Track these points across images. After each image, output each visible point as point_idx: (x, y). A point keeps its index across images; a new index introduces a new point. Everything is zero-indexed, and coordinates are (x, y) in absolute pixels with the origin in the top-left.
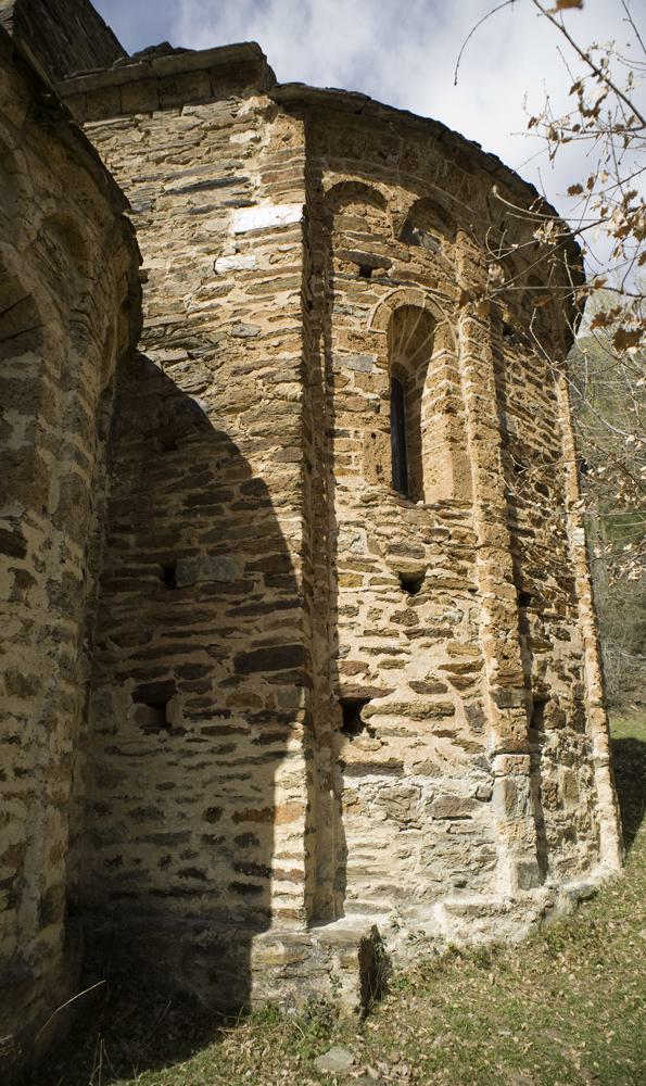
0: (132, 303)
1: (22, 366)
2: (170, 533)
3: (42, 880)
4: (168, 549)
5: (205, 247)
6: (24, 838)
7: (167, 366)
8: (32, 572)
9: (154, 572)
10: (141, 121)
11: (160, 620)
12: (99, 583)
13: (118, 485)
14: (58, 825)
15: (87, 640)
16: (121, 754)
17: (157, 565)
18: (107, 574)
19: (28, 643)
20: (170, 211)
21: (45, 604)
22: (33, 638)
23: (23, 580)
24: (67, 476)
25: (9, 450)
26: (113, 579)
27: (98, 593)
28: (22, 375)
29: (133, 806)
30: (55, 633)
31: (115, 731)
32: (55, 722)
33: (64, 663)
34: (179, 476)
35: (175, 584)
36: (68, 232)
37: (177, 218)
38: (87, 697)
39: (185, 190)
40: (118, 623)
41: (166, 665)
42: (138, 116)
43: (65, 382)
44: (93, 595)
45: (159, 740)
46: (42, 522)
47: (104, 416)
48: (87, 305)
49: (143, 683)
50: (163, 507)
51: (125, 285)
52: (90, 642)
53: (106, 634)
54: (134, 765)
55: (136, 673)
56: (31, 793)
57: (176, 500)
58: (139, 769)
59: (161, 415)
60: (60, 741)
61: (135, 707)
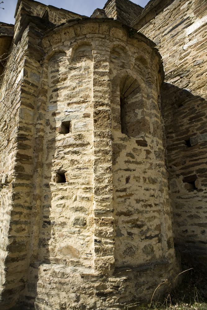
3: (167, 235)
4: (186, 135)
5: (179, 44)
7: (174, 83)
9: (183, 143)
11: (187, 157)
13: (166, 121)
14: (168, 219)
16: (182, 198)
18: (168, 146)
19: (152, 169)
21: (155, 158)
23: (148, 152)
24: (154, 122)
28: (137, 100)
29: (189, 214)
30: (159, 165)
31: (179, 192)
32: (163, 190)
39: (169, 32)
40: (174, 160)
41: (192, 170)
42: (151, 21)
43: (149, 97)
45: (194, 193)
46: (150, 136)
47: (159, 103)
48: (150, 76)
49: (186, 176)
50: (182, 123)
53: (171, 164)
54: (187, 202)
55: (183, 174)
57: (186, 120)
58: (188, 203)
59: (175, 97)
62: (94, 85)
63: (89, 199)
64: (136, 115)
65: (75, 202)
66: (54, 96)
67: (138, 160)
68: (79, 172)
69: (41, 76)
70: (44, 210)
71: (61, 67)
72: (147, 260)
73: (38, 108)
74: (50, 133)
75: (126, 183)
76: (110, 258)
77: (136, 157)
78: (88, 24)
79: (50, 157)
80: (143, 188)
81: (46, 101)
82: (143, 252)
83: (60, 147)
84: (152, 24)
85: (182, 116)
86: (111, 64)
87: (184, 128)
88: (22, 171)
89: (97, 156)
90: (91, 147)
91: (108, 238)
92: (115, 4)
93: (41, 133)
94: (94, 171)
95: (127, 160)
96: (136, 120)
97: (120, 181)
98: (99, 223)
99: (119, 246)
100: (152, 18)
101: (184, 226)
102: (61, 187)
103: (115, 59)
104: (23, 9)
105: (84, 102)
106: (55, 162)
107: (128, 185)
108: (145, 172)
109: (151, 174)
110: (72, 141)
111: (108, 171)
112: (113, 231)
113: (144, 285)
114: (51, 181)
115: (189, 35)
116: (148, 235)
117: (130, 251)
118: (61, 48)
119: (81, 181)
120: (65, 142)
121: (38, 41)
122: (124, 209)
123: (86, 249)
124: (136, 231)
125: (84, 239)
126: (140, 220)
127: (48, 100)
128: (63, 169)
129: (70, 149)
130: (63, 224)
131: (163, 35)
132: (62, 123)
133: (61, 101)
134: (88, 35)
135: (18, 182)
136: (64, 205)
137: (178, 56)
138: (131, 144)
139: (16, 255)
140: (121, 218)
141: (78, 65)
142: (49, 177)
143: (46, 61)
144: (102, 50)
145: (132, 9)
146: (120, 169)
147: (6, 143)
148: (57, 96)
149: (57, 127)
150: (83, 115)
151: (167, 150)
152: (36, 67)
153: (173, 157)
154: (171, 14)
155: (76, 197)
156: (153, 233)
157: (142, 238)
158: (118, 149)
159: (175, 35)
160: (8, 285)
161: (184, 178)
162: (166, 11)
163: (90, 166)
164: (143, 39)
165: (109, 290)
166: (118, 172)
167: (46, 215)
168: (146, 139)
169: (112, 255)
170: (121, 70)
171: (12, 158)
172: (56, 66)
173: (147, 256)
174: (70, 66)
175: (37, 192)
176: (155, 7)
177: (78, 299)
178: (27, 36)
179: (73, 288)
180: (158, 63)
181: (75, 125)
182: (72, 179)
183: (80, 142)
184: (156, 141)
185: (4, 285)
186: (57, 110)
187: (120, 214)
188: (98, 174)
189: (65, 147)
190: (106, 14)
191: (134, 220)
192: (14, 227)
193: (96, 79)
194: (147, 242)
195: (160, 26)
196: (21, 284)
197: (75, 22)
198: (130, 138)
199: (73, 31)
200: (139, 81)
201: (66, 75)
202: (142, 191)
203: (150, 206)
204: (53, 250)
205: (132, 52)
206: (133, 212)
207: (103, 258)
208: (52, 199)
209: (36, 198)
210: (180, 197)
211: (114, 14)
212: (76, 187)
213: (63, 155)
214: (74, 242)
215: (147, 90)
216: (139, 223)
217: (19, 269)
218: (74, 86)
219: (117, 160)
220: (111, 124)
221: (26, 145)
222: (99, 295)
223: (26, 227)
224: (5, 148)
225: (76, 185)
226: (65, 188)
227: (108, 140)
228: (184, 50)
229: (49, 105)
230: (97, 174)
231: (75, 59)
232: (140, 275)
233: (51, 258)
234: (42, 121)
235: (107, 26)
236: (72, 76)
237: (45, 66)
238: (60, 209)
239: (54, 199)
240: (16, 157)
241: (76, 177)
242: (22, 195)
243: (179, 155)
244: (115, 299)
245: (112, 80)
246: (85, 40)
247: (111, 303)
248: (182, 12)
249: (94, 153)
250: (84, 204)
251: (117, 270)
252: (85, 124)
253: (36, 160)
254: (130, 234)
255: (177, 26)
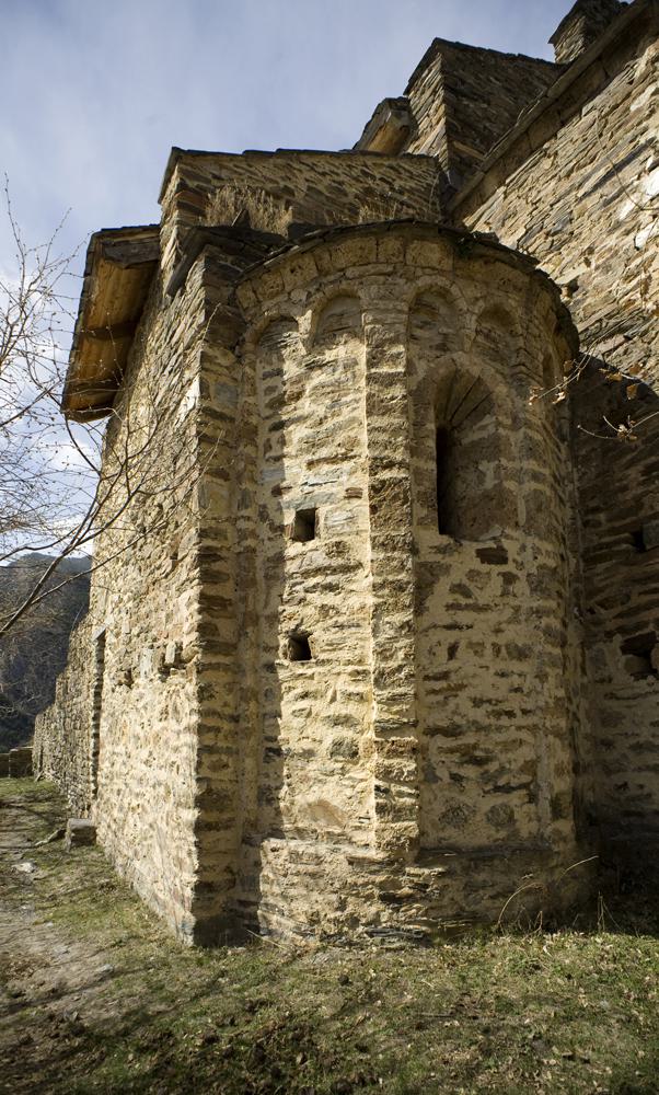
0: (562, 320)
1: (484, 428)
2: (633, 504)
3: (551, 787)
4: (634, 518)
5: (623, 229)
6: (535, 757)
7: (608, 356)
8: (515, 571)
9: (626, 541)
10: (548, 149)
11: (636, 581)
12: (581, 561)
13: (584, 474)
14: (559, 750)
15: (576, 609)
16: (618, 699)
17: (627, 535)
18: (587, 550)
19: (519, 622)
20: (586, 214)
21: (528, 592)
22: (523, 618)
23: (509, 579)
24: (529, 494)
25: (485, 490)
26: (592, 554)
27: (581, 568)
28: (484, 434)
29: (633, 741)
30: (538, 612)
31: (610, 680)
32: (546, 675)
33: (548, 631)
34: (633, 451)
35: (644, 547)
36: (497, 314)
37: (594, 217)
38: (583, 655)
39: (596, 187)
40: (601, 590)
41: (646, 619)
42: (545, 146)
43: (516, 422)
44: (577, 571)
45: (649, 684)
46: (515, 534)
47: (563, 421)
48: (522, 359)
49: (628, 637)
50: (625, 482)
51: (553, 316)
52: (579, 610)
53: (592, 601)
54: (629, 707)
55: (622, 630)
56: (535, 726)
57: (634, 473)
58: (633, 709)
59: (610, 402)
60: (552, 690)
61: (624, 658)
62: (369, 413)
63: (362, 698)
65: (333, 705)
66: (273, 443)
67: (481, 602)
68: (339, 635)
69: (239, 390)
70: (267, 723)
71: (287, 362)
72: (497, 840)
73: (239, 477)
74: (270, 539)
76: (410, 827)
78: (349, 242)
79: (275, 600)
80: (492, 671)
81: (256, 458)
82: (489, 820)
83: (295, 576)
84: (549, 157)
85: (624, 461)
86: (411, 345)
87: (629, 495)
88: (213, 635)
89: (379, 597)
90: (366, 573)
91: (404, 783)
92: (440, 77)
93: (250, 542)
94: (373, 631)
95: (451, 602)
97: (434, 654)
98: (386, 750)
99: (430, 803)
100: (547, 136)
101: (621, 774)
102: (301, 671)
103: (421, 328)
104: (182, 186)
105: (346, 458)
106: (284, 610)
107: (453, 665)
108: (498, 631)
109: (517, 634)
110: (320, 559)
111: (403, 632)
112: (416, 768)
113: (483, 887)
114: (278, 658)
116: (501, 782)
117: (454, 815)
118: (285, 309)
119: (345, 655)
120: (306, 562)
121: (227, 292)
122: (443, 720)
123: (359, 807)
124: (470, 771)
125: (353, 787)
126: (482, 746)
127: (261, 454)
128: (303, 628)
129: (319, 579)
130: (309, 754)
131: (579, 195)
132: (297, 513)
133: (291, 457)
134: (351, 269)
135: (206, 661)
136: (307, 711)
137: (620, 270)
138: (465, 560)
139: (213, 817)
140: (437, 736)
141: (329, 355)
142: (272, 648)
143: (249, 346)
144: (387, 311)
145: (496, 79)
146: (435, 626)
147: (167, 564)
148: (283, 442)
149: (285, 523)
150: (344, 494)
151: (585, 561)
152: (227, 368)
153: (598, 582)
154: (605, 127)
155: (335, 692)
156: (516, 780)
157: (486, 789)
158: (429, 575)
159: (614, 198)
160: (204, 873)
161: (626, 641)
162: (588, 112)
163: (364, 619)
164: (499, 255)
165: (406, 890)
166: (431, 632)
167: (269, 734)
168: (506, 544)
169: (413, 820)
171: (189, 605)
172: (274, 360)
173: (498, 831)
174: (310, 359)
175: (249, 682)
176: (557, 100)
177: (342, 906)
178: (202, 286)
179: (332, 885)
180: (551, 308)
181: (326, 519)
182: (324, 651)
183: (340, 561)
184: (532, 548)
185: (196, 872)
186: (284, 480)
187: (432, 732)
188: (382, 638)
189: (306, 574)
190: (414, 113)
191: (467, 746)
192: (207, 760)
193: (374, 395)
194: (499, 800)
195: (572, 164)
196: (229, 876)
197: (316, 241)
198: (461, 545)
199: (312, 263)
200: (489, 382)
201: (300, 385)
202: (489, 677)
203: (510, 714)
204: (289, 810)
205: (469, 299)
206: (465, 729)
207: (393, 825)
208: (281, 698)
209: (247, 695)
210: (612, 694)
211: (437, 116)
212: (334, 671)
213: (302, 594)
214: (333, 792)
215: (513, 402)
216: (478, 753)
217: (222, 847)
218: (322, 414)
219: (427, 604)
220: (411, 514)
221: (218, 572)
222: (383, 898)
223: (230, 759)
224: (166, 577)
225: (333, 665)
226: (309, 672)
227: (405, 556)
228: (638, 249)
229: (264, 467)
230: (379, 639)
231: (321, 338)
232: (476, 867)
233: (287, 826)
234: (249, 509)
235: (396, 239)
236: (315, 388)
237: (247, 361)
238: (301, 720)
239: (286, 698)
240: (199, 603)
241: (334, 646)
242: (217, 689)
243: (614, 575)
244: (419, 909)
245: (416, 391)
246: (344, 285)
247: (411, 916)
248: (634, 121)
249: (371, 588)
250: (351, 709)
251: (423, 852)
252: (350, 515)
253: (242, 607)
254: (456, 778)
255: (618, 168)
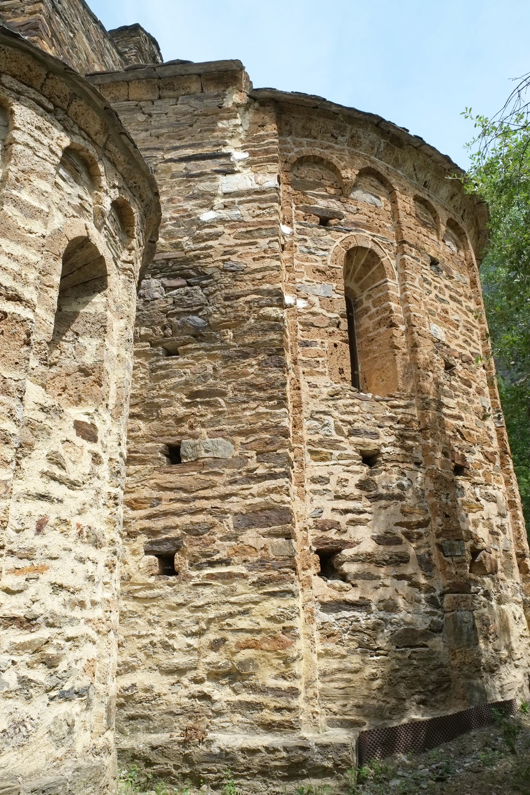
23: (96, 459)
64: (81, 351)
67: (72, 477)
75: (36, 534)
77: (69, 465)
96: (77, 364)
115: (225, 194)
134: (9, 78)
170: (73, 216)
173: (462, 501)
203: (82, 604)
